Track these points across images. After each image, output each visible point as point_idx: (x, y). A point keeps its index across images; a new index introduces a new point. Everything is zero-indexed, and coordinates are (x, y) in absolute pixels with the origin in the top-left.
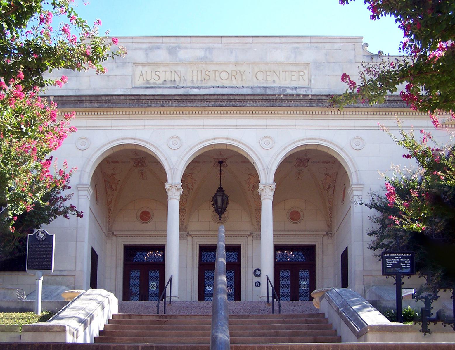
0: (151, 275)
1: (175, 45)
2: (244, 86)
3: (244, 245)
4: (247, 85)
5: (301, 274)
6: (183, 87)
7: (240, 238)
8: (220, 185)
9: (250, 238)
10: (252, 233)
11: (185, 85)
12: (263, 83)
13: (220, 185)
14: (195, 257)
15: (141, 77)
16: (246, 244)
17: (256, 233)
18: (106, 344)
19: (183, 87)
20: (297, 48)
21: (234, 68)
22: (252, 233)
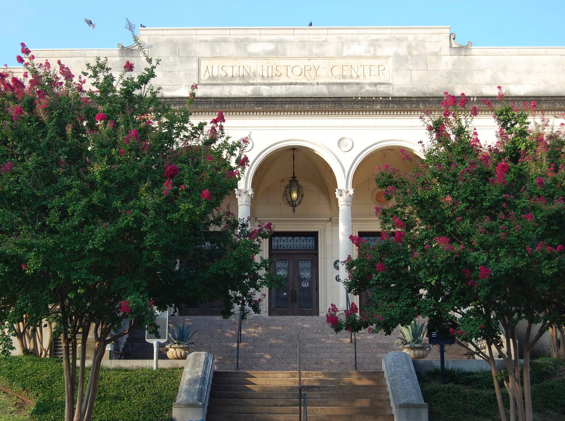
0: (302, 266)
1: (244, 37)
2: (319, 82)
3: (322, 232)
4: (322, 81)
5: (301, 265)
6: (253, 84)
7: (316, 223)
8: (294, 174)
9: (329, 224)
10: (331, 219)
11: (255, 81)
12: (340, 79)
13: (294, 174)
14: (323, 285)
15: (207, 72)
16: (324, 231)
17: (334, 220)
18: (155, 349)
19: (253, 84)
20: (377, 40)
21: (307, 62)
22: (331, 219)
